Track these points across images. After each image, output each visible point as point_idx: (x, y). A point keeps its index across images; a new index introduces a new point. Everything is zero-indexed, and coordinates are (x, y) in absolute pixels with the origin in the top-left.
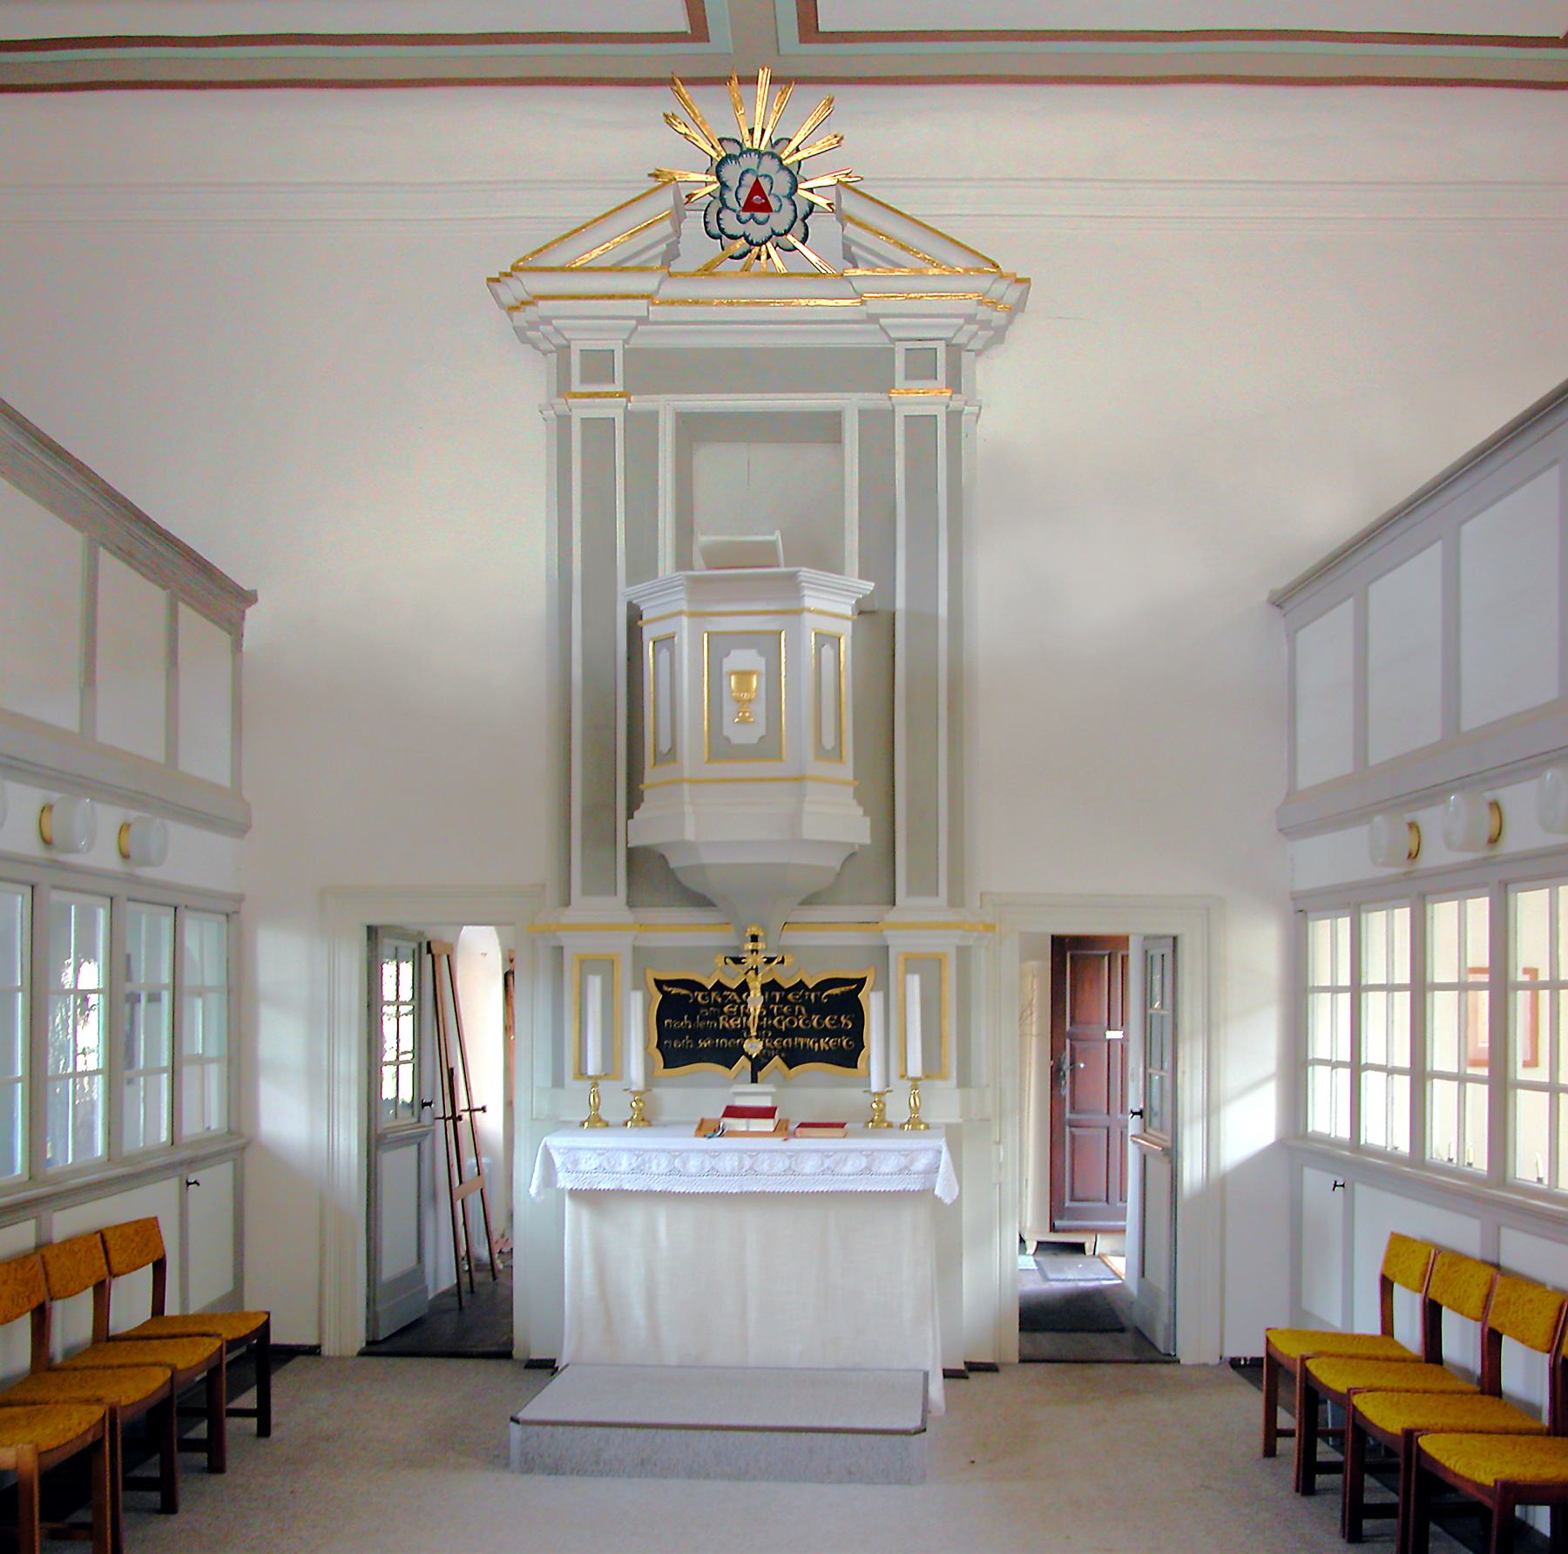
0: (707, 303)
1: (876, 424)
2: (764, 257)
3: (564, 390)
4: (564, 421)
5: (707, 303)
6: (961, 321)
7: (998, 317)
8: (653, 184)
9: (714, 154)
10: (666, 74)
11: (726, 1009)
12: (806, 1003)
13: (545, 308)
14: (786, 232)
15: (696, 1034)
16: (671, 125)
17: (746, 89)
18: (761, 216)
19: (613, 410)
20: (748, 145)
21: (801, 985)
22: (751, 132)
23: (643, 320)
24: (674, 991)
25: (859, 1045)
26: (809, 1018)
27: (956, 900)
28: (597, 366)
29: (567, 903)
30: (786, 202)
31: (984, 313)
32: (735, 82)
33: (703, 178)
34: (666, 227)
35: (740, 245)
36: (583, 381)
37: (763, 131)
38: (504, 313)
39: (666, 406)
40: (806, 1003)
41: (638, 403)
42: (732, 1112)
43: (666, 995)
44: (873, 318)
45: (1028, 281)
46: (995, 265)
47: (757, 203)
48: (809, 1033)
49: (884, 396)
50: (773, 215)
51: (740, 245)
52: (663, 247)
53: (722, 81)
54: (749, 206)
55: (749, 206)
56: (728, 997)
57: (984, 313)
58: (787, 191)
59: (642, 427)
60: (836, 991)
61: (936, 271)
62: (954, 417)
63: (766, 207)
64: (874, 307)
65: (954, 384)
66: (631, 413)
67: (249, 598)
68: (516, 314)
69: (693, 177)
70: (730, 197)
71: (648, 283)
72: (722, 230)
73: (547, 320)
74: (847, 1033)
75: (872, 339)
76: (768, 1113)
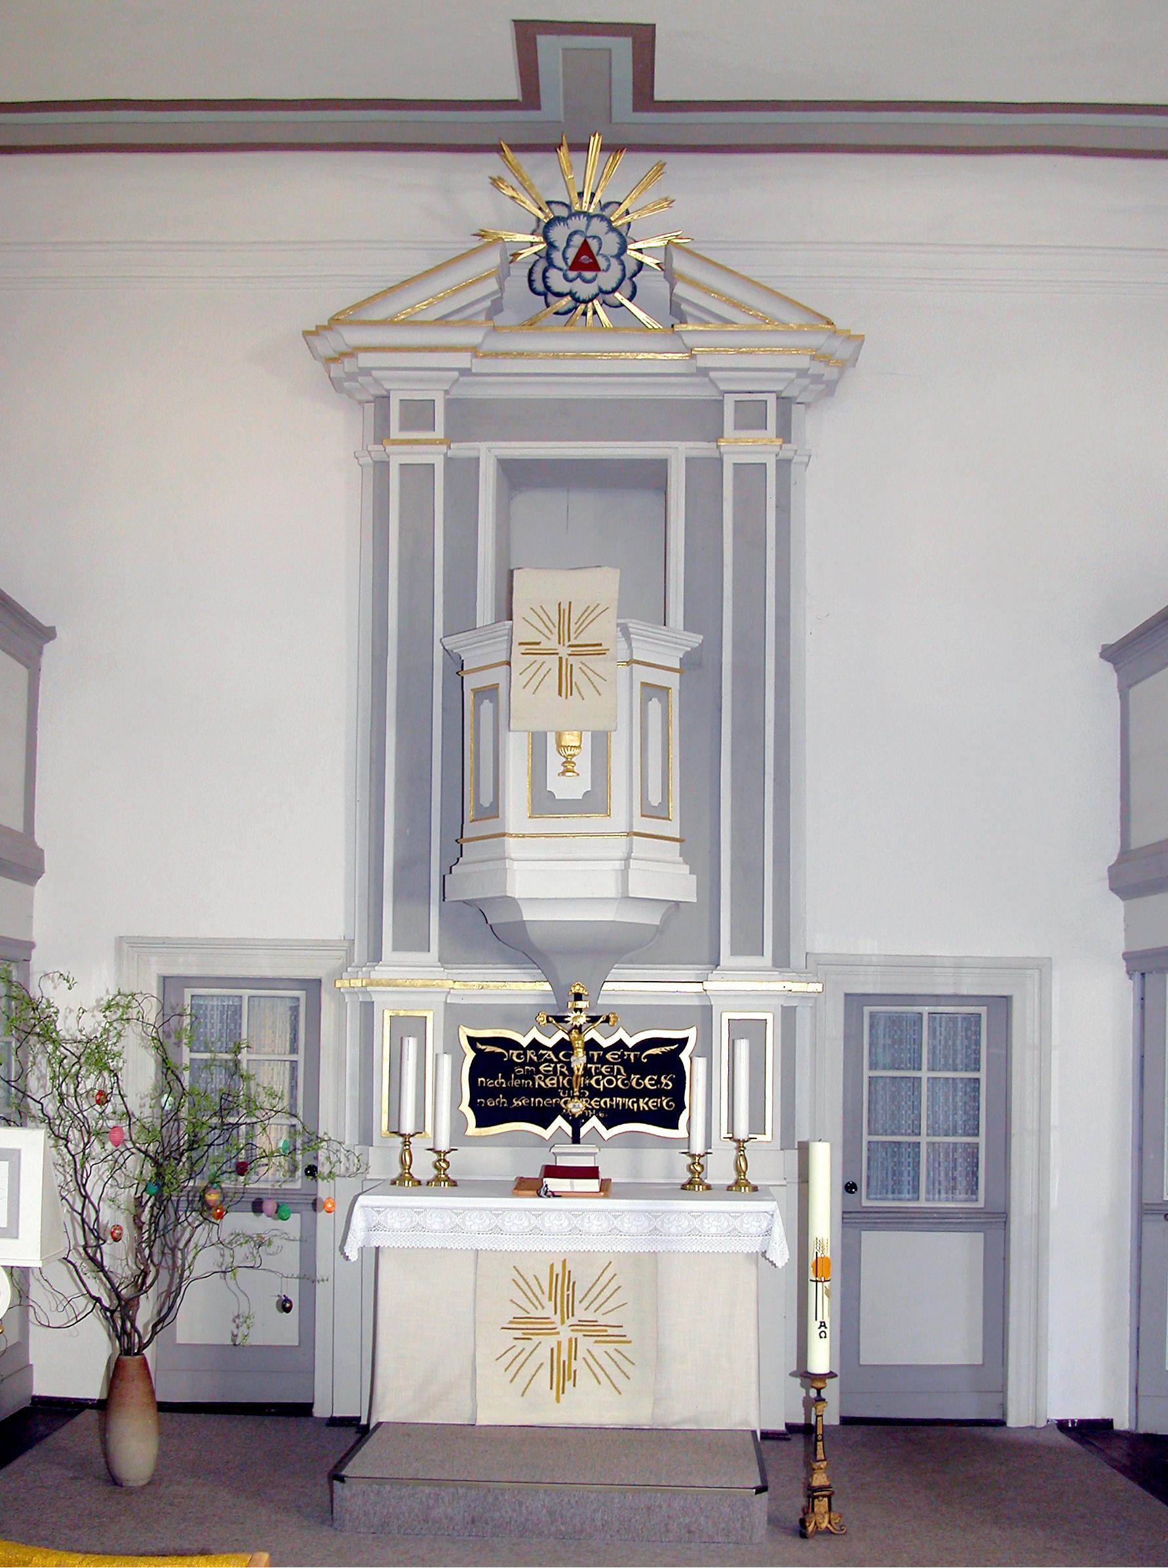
0: (532, 355)
1: (706, 473)
2: (590, 314)
3: (382, 434)
4: (382, 467)
5: (532, 355)
6: (793, 375)
7: (830, 373)
8: (476, 243)
9: (540, 215)
10: (493, 141)
11: (542, 1068)
12: (625, 1063)
13: (365, 360)
14: (614, 290)
15: (511, 1093)
16: (498, 188)
17: (579, 157)
18: (588, 275)
19: (435, 457)
20: (577, 207)
22: (581, 195)
23: (465, 372)
24: (489, 1049)
25: (678, 1094)
26: (628, 1078)
28: (418, 414)
29: (376, 956)
30: (614, 262)
31: (817, 368)
32: (564, 149)
33: (531, 238)
34: (492, 285)
35: (566, 302)
36: (403, 428)
37: (593, 195)
38: (319, 365)
39: (488, 454)
40: (625, 1063)
41: (460, 449)
42: (552, 1171)
44: (704, 372)
45: (861, 338)
46: (829, 323)
47: (585, 261)
48: (630, 1093)
49: (713, 445)
50: (600, 274)
51: (566, 302)
52: (488, 303)
53: (554, 148)
54: (577, 265)
55: (577, 265)
57: (817, 368)
58: (616, 252)
59: (463, 474)
61: (769, 327)
62: (784, 465)
63: (595, 267)
64: (702, 362)
65: (784, 432)
66: (451, 459)
67: (48, 634)
68: (333, 366)
69: (520, 237)
70: (557, 257)
71: (473, 337)
72: (548, 288)
73: (366, 372)
74: (666, 1093)
75: (699, 392)
76: (590, 1173)
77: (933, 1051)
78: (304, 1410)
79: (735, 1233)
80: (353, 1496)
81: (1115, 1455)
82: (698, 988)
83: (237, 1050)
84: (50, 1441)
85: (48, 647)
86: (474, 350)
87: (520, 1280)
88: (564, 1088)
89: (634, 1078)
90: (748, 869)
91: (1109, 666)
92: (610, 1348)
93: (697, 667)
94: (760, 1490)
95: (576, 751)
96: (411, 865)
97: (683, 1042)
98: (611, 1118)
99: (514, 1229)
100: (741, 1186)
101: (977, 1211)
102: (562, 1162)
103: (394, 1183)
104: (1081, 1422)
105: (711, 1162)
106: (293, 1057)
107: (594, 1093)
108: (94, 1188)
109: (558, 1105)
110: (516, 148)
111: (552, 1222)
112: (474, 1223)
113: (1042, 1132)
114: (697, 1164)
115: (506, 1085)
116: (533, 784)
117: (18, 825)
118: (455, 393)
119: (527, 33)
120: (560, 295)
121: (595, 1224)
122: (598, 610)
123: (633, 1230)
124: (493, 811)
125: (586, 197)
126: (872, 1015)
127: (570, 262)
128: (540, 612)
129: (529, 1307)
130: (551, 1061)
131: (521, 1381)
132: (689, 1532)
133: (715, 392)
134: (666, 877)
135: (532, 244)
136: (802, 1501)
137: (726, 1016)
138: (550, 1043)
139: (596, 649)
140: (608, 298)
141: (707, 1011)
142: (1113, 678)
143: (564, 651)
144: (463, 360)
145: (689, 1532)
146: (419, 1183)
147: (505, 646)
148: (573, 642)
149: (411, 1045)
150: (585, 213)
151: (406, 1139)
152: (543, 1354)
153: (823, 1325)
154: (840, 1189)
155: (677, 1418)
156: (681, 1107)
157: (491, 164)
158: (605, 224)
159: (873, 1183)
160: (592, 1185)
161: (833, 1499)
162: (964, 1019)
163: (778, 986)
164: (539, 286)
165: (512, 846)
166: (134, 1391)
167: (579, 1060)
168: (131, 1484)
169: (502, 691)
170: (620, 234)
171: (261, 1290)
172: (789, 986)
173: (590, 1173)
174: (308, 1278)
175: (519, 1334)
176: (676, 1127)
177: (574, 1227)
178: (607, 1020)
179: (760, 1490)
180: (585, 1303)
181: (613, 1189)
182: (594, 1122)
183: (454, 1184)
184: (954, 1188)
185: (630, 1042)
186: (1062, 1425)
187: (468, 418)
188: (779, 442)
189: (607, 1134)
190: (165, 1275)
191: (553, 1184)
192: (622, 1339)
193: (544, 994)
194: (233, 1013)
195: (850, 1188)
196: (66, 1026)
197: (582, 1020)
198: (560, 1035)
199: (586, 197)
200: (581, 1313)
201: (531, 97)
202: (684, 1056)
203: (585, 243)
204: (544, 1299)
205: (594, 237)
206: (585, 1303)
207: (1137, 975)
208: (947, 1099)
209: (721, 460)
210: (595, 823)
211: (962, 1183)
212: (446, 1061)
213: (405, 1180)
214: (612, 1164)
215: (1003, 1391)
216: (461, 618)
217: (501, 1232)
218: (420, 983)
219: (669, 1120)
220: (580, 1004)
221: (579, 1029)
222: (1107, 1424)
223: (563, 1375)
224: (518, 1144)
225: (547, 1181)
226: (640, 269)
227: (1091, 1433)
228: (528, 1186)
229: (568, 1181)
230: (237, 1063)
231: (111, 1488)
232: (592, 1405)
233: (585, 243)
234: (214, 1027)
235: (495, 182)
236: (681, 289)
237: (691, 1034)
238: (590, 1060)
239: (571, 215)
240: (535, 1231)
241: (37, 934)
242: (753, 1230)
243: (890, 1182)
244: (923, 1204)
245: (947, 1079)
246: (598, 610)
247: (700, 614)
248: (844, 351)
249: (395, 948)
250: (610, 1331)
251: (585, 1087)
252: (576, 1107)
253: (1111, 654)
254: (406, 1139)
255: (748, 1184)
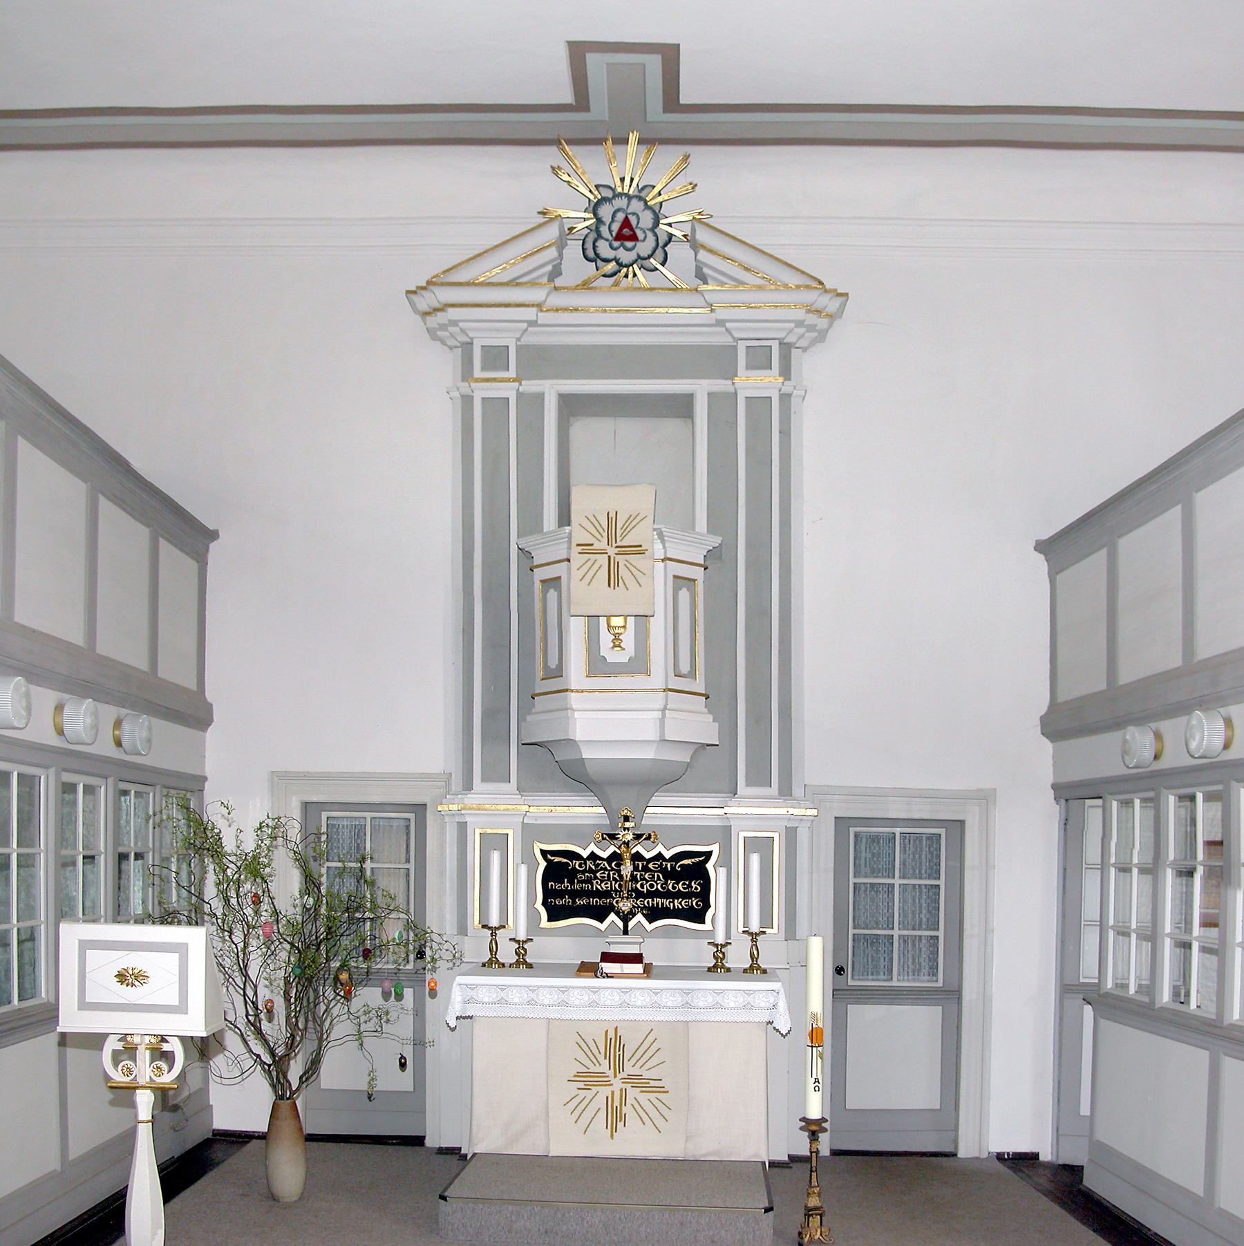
1: (722, 404)
2: (631, 275)
3: (467, 373)
4: (467, 400)
8: (541, 219)
9: (592, 197)
13: (453, 313)
14: (649, 257)
17: (619, 148)
18: (629, 244)
19: (508, 391)
20: (619, 190)
22: (622, 180)
23: (533, 323)
24: (557, 859)
25: (704, 895)
26: (666, 883)
28: (495, 357)
29: (468, 786)
30: (650, 234)
31: (812, 319)
32: (609, 143)
34: (552, 253)
35: (611, 267)
36: (483, 369)
37: (632, 180)
38: (418, 318)
39: (551, 389)
41: (530, 386)
42: (607, 957)
44: (720, 323)
45: (846, 295)
46: (821, 283)
47: (627, 234)
49: (729, 382)
50: (639, 244)
51: (611, 267)
52: (549, 268)
53: (600, 141)
54: (620, 237)
55: (620, 237)
62: (785, 398)
63: (634, 238)
64: (721, 314)
65: (786, 372)
67: (213, 535)
68: (428, 318)
70: (604, 230)
71: (537, 295)
73: (454, 323)
75: (719, 338)
76: (636, 958)
77: (903, 863)
78: (418, 1141)
79: (748, 1007)
80: (454, 1212)
81: (1041, 1181)
82: (721, 812)
83: (363, 860)
84: (225, 1166)
85: (213, 546)
86: (539, 306)
88: (616, 891)
89: (671, 883)
90: (759, 717)
91: (1042, 557)
92: (652, 1096)
93: (716, 559)
94: (767, 1210)
95: (622, 630)
96: (495, 714)
97: (708, 855)
98: (651, 918)
99: (577, 1002)
100: (755, 969)
101: (936, 991)
102: (615, 949)
103: (484, 965)
104: (1014, 1154)
105: (729, 950)
106: (407, 866)
107: (639, 895)
108: (253, 972)
109: (611, 904)
110: (570, 142)
111: (607, 998)
112: (545, 997)
113: (987, 931)
114: (720, 950)
115: (569, 887)
116: (589, 650)
117: (192, 685)
118: (524, 341)
119: (578, 51)
120: (607, 261)
121: (639, 999)
122: (639, 518)
124: (558, 672)
125: (627, 181)
126: (856, 835)
128: (593, 520)
130: (606, 869)
133: (730, 339)
134: (696, 724)
135: (585, 219)
136: (800, 1217)
137: (742, 835)
138: (605, 855)
139: (638, 550)
140: (645, 263)
141: (727, 830)
142: (1044, 566)
143: (612, 551)
144: (530, 314)
146: (503, 965)
147: (566, 546)
148: (619, 544)
149: (496, 857)
150: (627, 195)
151: (494, 931)
152: (600, 1101)
153: (817, 1081)
154: (830, 971)
155: (704, 1152)
156: (707, 906)
157: (551, 155)
158: (642, 203)
159: (857, 966)
160: (638, 968)
162: (928, 838)
163: (783, 811)
165: (574, 699)
166: (287, 1126)
167: (627, 869)
168: (286, 1200)
169: (564, 581)
170: (654, 211)
171: (384, 1051)
172: (792, 811)
173: (636, 958)
174: (420, 1043)
175: (581, 1085)
176: (703, 922)
177: (622, 999)
178: (649, 838)
179: (767, 1210)
181: (654, 971)
182: (639, 917)
183: (530, 966)
184: (919, 971)
185: (667, 855)
186: (1000, 1157)
187: (538, 360)
188: (781, 380)
189: (649, 927)
190: (311, 1034)
191: (608, 967)
192: (662, 1090)
193: (600, 816)
194: (359, 832)
195: (839, 971)
196: (229, 845)
197: (630, 837)
198: (612, 849)
199: (627, 181)
200: (629, 1069)
201: (582, 101)
202: (709, 866)
203: (626, 219)
204: (601, 1058)
205: (634, 214)
207: (1063, 801)
208: (914, 900)
209: (736, 393)
210: (639, 681)
211: (925, 970)
212: (523, 869)
213: (492, 963)
214: (653, 952)
215: (956, 1129)
216: (532, 524)
217: (567, 1005)
218: (503, 807)
219: (697, 915)
220: (627, 825)
221: (627, 844)
222: (1034, 1157)
223: (615, 1118)
224: (581, 937)
225: (603, 965)
226: (670, 240)
227: (1023, 1162)
228: (588, 969)
229: (618, 965)
230: (362, 870)
231: (271, 1203)
232: (638, 1141)
233: (626, 219)
234: (345, 839)
235: (555, 170)
236: (703, 256)
237: (715, 848)
238: (636, 868)
240: (593, 1004)
241: (210, 768)
242: (763, 1005)
243: (870, 966)
244: (895, 983)
245: (914, 885)
246: (639, 518)
247: (720, 517)
248: (833, 305)
249: (484, 780)
250: (652, 1083)
251: (632, 890)
252: (625, 906)
253: (1043, 547)
254: (494, 931)
255: (759, 968)
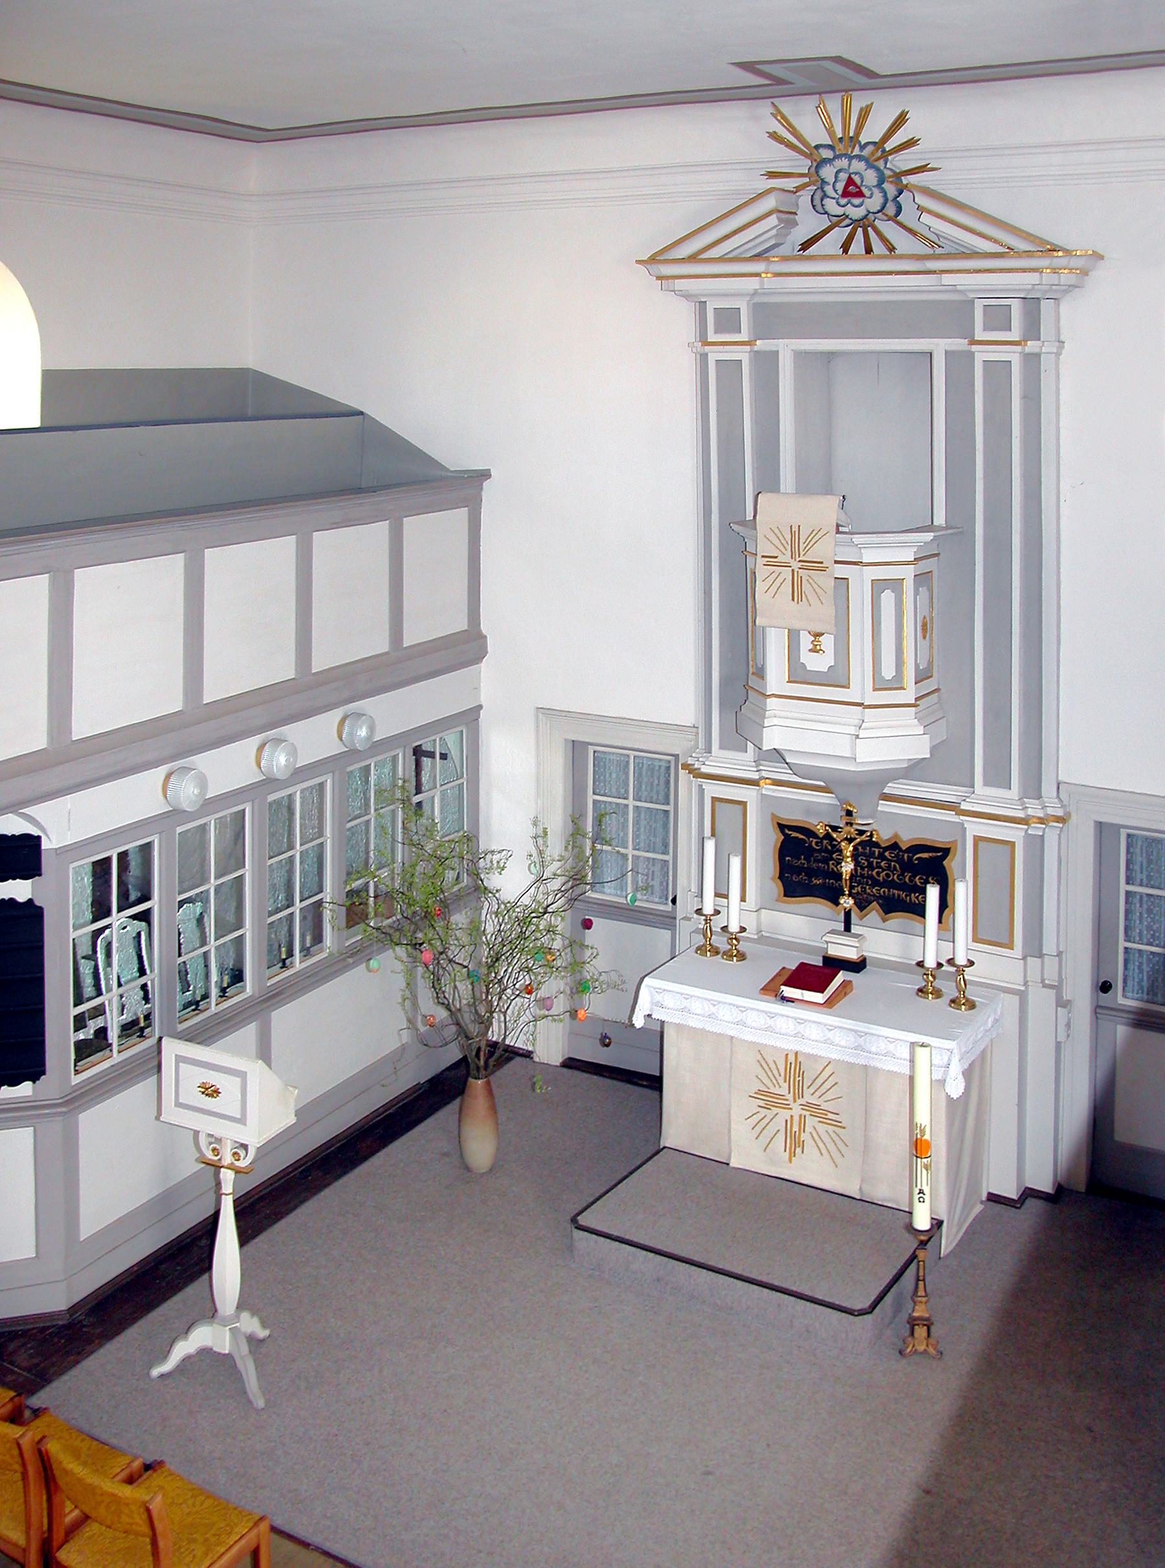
1: (960, 363)
4: (704, 357)
15: (811, 873)
18: (856, 201)
19: (743, 355)
21: (895, 846)
24: (794, 834)
26: (902, 874)
27: (1033, 788)
28: (728, 320)
30: (875, 190)
39: (786, 349)
40: (900, 861)
43: (786, 836)
55: (846, 194)
56: (828, 847)
59: (767, 364)
60: (925, 855)
63: (860, 194)
70: (829, 189)
87: (763, 1062)
89: (908, 875)
93: (957, 532)
99: (754, 1024)
112: (725, 1013)
123: (843, 1043)
127: (840, 192)
128: (776, 531)
129: (769, 1084)
131: (764, 1139)
132: (808, 1331)
145: (808, 1331)
152: (779, 1123)
159: (1130, 983)
161: (933, 1328)
164: (819, 208)
175: (762, 1103)
180: (812, 1090)
192: (838, 1124)
195: (1105, 987)
200: (807, 1098)
205: (856, 174)
206: (812, 1090)
217: (744, 1025)
223: (795, 1143)
239: (836, 157)
240: (769, 1029)
241: (483, 700)
250: (830, 1116)
